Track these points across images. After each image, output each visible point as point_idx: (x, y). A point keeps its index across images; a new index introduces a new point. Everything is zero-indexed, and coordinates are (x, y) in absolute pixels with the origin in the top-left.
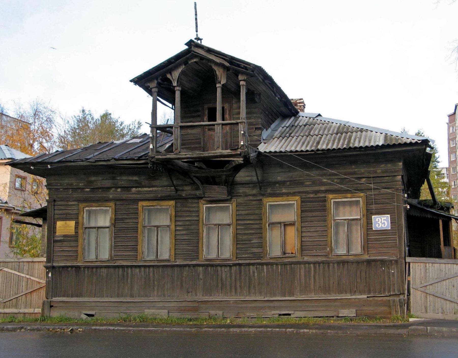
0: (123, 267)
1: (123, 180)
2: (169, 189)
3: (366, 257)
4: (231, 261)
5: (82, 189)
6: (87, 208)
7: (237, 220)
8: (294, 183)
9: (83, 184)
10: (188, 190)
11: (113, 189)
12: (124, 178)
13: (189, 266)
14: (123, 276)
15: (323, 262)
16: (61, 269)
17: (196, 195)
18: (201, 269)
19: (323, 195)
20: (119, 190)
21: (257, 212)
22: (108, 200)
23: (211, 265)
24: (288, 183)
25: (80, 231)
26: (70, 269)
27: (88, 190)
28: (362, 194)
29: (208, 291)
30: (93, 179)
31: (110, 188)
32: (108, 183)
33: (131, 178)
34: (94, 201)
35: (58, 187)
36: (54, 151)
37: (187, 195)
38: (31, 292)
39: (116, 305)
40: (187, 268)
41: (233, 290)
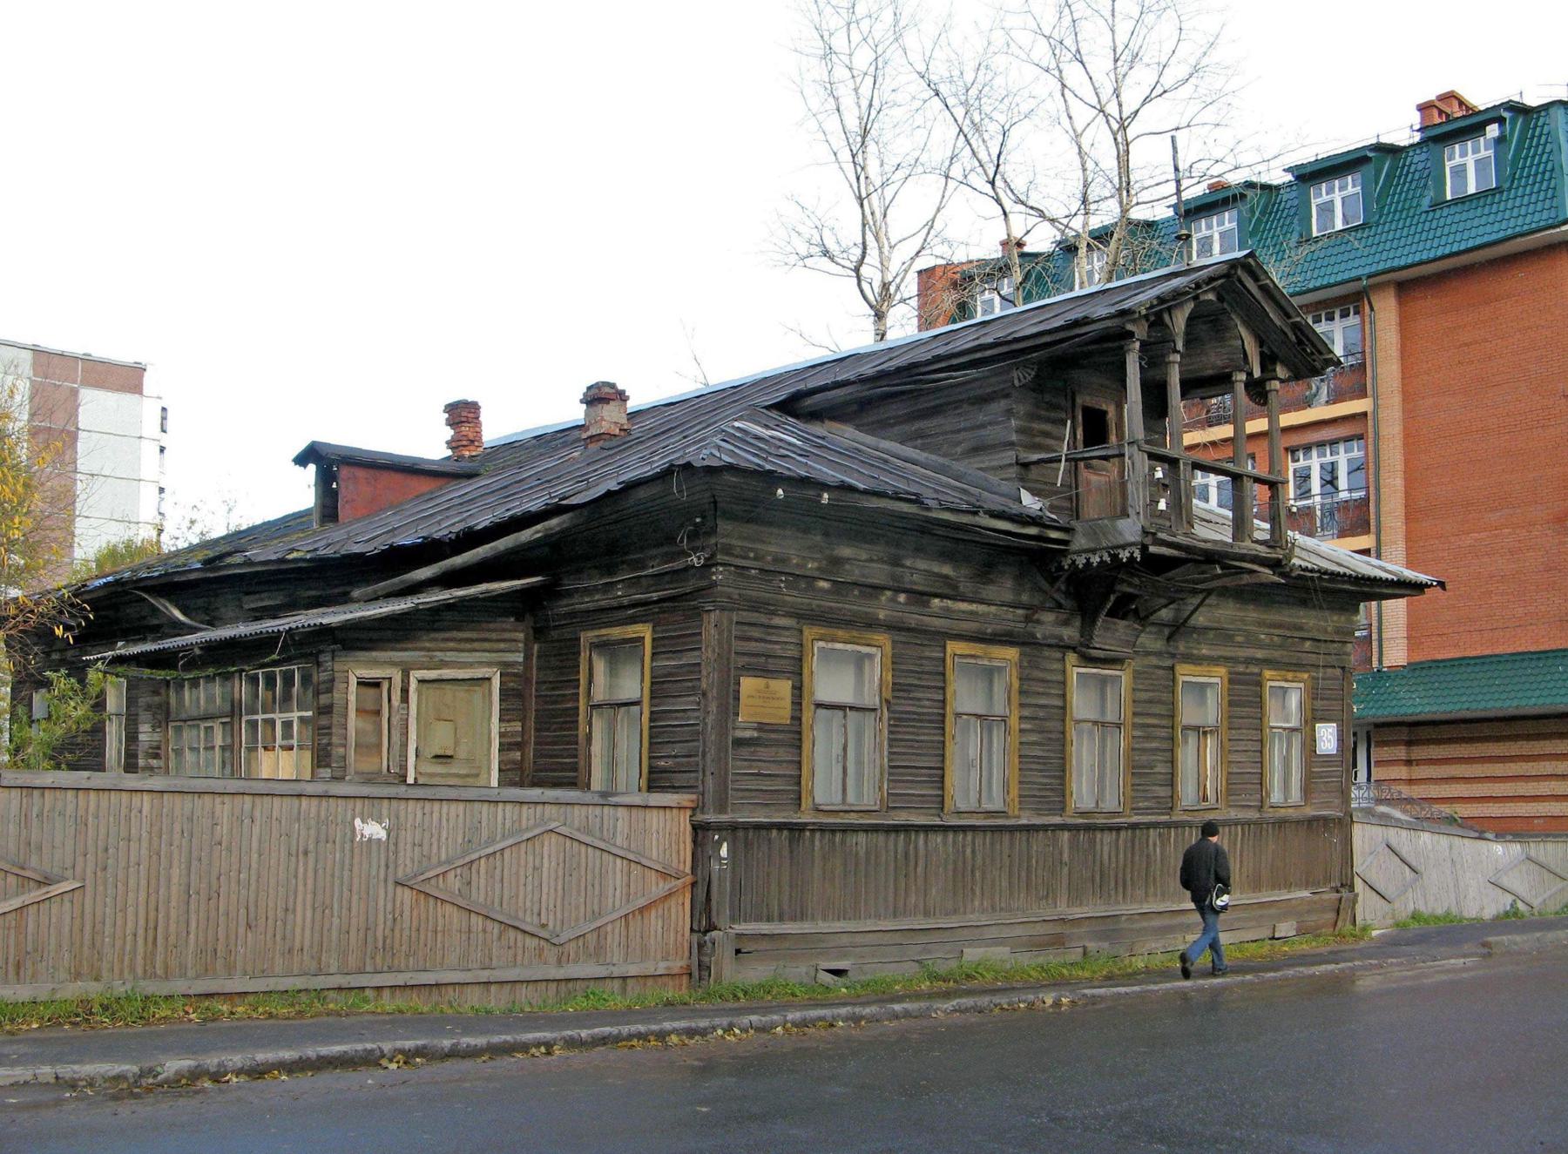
1: (921, 568)
2: (1009, 614)
3: (1310, 812)
4: (1008, 817)
6: (822, 644)
7: (1135, 714)
8: (1223, 635)
9: (816, 565)
10: (1049, 625)
11: (889, 593)
12: (922, 564)
13: (1045, 828)
16: (751, 834)
17: (1061, 639)
18: (1065, 836)
19: (1256, 670)
20: (902, 598)
21: (1165, 696)
22: (871, 624)
24: (1211, 634)
25: (807, 716)
26: (774, 833)
27: (824, 585)
28: (1306, 676)
30: (846, 551)
31: (884, 588)
32: (878, 573)
33: (936, 569)
36: (1129, 530)
37: (1045, 638)
38: (642, 910)
39: (897, 938)
41: (1121, 890)
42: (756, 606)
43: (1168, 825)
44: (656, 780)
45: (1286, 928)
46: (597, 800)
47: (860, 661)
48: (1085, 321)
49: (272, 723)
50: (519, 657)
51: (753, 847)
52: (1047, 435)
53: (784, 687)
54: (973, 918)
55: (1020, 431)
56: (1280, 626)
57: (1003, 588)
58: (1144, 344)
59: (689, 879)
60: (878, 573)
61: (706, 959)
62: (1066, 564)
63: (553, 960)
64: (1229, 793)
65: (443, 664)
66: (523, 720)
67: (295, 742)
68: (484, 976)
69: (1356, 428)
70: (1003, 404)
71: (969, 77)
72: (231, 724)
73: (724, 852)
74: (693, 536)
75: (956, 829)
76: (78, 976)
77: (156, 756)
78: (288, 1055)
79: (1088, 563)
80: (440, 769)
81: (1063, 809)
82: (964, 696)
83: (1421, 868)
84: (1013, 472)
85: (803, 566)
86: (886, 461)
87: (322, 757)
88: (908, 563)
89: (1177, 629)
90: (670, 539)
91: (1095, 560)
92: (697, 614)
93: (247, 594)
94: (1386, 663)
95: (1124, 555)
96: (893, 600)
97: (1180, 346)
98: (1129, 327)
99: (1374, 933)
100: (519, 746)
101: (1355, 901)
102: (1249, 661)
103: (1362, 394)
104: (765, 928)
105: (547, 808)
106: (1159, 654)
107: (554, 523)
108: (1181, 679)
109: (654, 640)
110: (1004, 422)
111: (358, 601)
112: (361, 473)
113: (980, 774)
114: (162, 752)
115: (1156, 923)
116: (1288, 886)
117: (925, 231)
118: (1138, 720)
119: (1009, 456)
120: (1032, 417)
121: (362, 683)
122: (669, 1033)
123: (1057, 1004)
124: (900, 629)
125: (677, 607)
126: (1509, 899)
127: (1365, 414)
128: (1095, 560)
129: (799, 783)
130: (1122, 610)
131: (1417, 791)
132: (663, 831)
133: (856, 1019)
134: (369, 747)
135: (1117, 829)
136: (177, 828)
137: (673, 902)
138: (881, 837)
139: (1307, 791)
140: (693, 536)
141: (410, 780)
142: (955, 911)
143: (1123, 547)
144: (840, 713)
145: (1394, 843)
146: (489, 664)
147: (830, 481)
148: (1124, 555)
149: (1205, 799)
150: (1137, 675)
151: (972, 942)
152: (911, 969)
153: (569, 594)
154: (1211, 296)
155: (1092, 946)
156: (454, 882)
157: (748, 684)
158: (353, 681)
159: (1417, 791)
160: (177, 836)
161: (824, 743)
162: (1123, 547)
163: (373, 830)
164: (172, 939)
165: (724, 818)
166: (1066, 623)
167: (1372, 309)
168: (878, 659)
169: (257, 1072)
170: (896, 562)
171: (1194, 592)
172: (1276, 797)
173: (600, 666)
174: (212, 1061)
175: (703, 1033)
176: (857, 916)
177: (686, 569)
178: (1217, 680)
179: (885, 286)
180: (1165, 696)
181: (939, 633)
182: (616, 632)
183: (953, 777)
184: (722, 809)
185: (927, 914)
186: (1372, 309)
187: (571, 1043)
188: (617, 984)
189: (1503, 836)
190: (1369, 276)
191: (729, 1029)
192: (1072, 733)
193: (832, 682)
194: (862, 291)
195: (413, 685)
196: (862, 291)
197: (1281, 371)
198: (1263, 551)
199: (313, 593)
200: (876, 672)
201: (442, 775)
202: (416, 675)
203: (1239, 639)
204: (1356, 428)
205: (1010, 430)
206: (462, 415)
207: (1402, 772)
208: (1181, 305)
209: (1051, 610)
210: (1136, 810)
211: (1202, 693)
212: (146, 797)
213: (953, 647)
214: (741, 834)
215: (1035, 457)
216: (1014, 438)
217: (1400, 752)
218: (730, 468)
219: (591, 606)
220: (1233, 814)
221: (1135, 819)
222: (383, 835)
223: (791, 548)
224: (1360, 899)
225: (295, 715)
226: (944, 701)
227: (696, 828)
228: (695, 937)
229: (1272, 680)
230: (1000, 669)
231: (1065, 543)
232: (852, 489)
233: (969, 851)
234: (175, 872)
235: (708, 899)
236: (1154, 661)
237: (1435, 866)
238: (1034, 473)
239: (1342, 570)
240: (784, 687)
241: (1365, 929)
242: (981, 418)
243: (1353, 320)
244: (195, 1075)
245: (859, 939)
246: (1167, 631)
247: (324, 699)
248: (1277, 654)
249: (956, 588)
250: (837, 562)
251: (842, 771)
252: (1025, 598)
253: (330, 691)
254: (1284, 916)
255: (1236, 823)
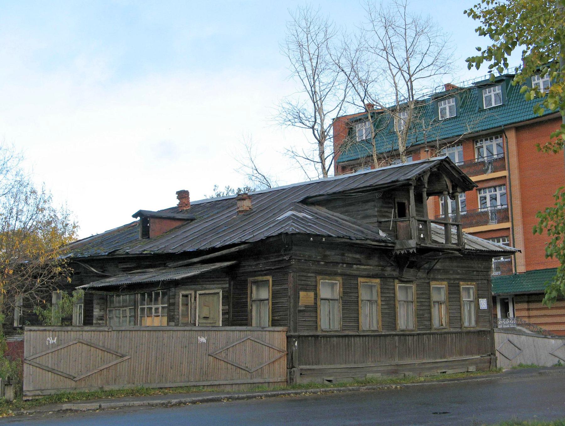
0: (351, 336)
1: (350, 256)
2: (377, 268)
3: (478, 329)
5: (318, 262)
6: (322, 281)
7: (417, 298)
8: (446, 272)
10: (389, 271)
12: (350, 255)
13: (390, 335)
14: (348, 344)
15: (460, 333)
18: (397, 338)
19: (457, 282)
20: (345, 265)
21: (427, 292)
22: (336, 274)
23: (404, 335)
25: (318, 303)
27: (322, 263)
29: (401, 357)
30: (328, 253)
31: (339, 263)
32: (338, 258)
34: (326, 274)
35: (300, 258)
36: (413, 243)
38: (273, 362)
39: (346, 370)
40: (389, 337)
42: (303, 270)
43: (430, 334)
44: (274, 323)
45: (472, 368)
46: (261, 329)
47: (333, 285)
48: (397, 181)
49: (151, 309)
50: (227, 285)
51: (305, 343)
52: (387, 212)
53: (312, 294)
54: (369, 364)
55: (378, 211)
56: (465, 267)
57: (374, 261)
58: (415, 187)
59: (286, 353)
60: (338, 258)
61: (292, 377)
62: (394, 253)
63: (249, 377)
64: (450, 323)
65: (205, 289)
66: (229, 305)
67: (160, 314)
68: (231, 382)
69: (501, 182)
70: (373, 203)
71: (353, 55)
72: (135, 309)
73: (296, 344)
74: (285, 250)
75: (363, 336)
76: (129, 383)
77: (101, 320)
78: (200, 398)
79: (400, 253)
80: (204, 321)
81: (396, 329)
82: (364, 294)
83: (522, 348)
84: (376, 224)
85: (317, 258)
86: (337, 221)
87: (171, 319)
88: (346, 255)
89: (430, 271)
90: (279, 251)
91: (403, 252)
92: (287, 273)
93: (120, 263)
94: (518, 271)
95: (411, 251)
96: (342, 266)
97: (426, 186)
98: (410, 183)
99: (504, 370)
100: (227, 313)
101: (496, 359)
102: (455, 279)
103: (504, 169)
104: (308, 367)
105: (236, 333)
106: (424, 278)
107: (242, 246)
108: (432, 286)
109: (273, 281)
110: (373, 209)
111: (170, 268)
112: (157, 220)
113: (370, 318)
114: (105, 319)
115: (427, 366)
116: (472, 354)
117: (338, 108)
118: (419, 300)
119: (375, 219)
120: (382, 207)
121: (183, 296)
122: (291, 393)
123: (396, 388)
124: (345, 275)
125: (280, 271)
126: (557, 359)
127: (505, 177)
128: (403, 252)
129: (317, 323)
130: (412, 265)
131: (533, 321)
132: (278, 338)
133: (340, 391)
134: (185, 315)
135: (413, 335)
136: (154, 341)
137: (282, 360)
138: (341, 339)
139: (477, 322)
140: (285, 250)
141: (197, 325)
142: (364, 362)
143: (411, 248)
144: (328, 301)
145: (511, 340)
146: (219, 288)
147: (325, 234)
148: (411, 251)
149: (442, 325)
150: (417, 285)
151: (369, 372)
152: (351, 380)
153: (244, 266)
154: (435, 170)
155: (407, 373)
156: (223, 355)
157: (302, 294)
158: (181, 295)
159: (533, 321)
160: (154, 343)
161: (323, 310)
162: (411, 248)
163: (203, 340)
164: (152, 372)
165: (297, 334)
166: (394, 270)
167: (506, 137)
168: (338, 284)
169: (194, 402)
170: (343, 255)
171: (434, 259)
172: (466, 324)
173: (254, 288)
174: (183, 400)
175: (299, 394)
176: (334, 363)
177: (282, 260)
178: (444, 286)
179: (323, 132)
180: (427, 292)
181: (355, 276)
182: (260, 278)
183: (362, 319)
184: (295, 330)
185: (355, 363)
186: (506, 137)
187: (267, 396)
188: (267, 384)
189: (554, 336)
190: (504, 126)
191: (306, 393)
192: (397, 305)
193: (325, 292)
194: (315, 135)
195: (198, 296)
196: (315, 135)
197: (458, 190)
198: (455, 246)
199: (148, 263)
200: (338, 289)
201: (205, 323)
202: (198, 292)
203: (451, 272)
204: (501, 182)
205: (374, 211)
206: (183, 195)
207: (525, 313)
208: (426, 174)
209: (389, 266)
210: (419, 329)
211: (439, 290)
212: (147, 332)
213: (360, 280)
214: (300, 338)
215: (383, 220)
216: (376, 214)
217: (525, 306)
218: (299, 233)
219: (251, 270)
220: (452, 330)
221: (419, 332)
222: (205, 341)
223: (314, 254)
224: (498, 359)
225: (160, 306)
226: (358, 297)
227: (288, 337)
228: (289, 370)
229: (463, 285)
230: (375, 286)
231: (393, 247)
232: (331, 236)
233: (367, 343)
234: (153, 353)
235: (292, 358)
236: (423, 281)
237: (521, 344)
238: (383, 225)
239: (484, 249)
240: (312, 294)
241: (500, 369)
242: (366, 207)
243: (500, 140)
244: (180, 403)
245: (335, 370)
246: (427, 271)
247: (171, 301)
248: (463, 277)
249: (360, 261)
250: (325, 256)
251: (329, 319)
252: (382, 263)
253: (174, 298)
254: (471, 364)
255: (453, 333)
